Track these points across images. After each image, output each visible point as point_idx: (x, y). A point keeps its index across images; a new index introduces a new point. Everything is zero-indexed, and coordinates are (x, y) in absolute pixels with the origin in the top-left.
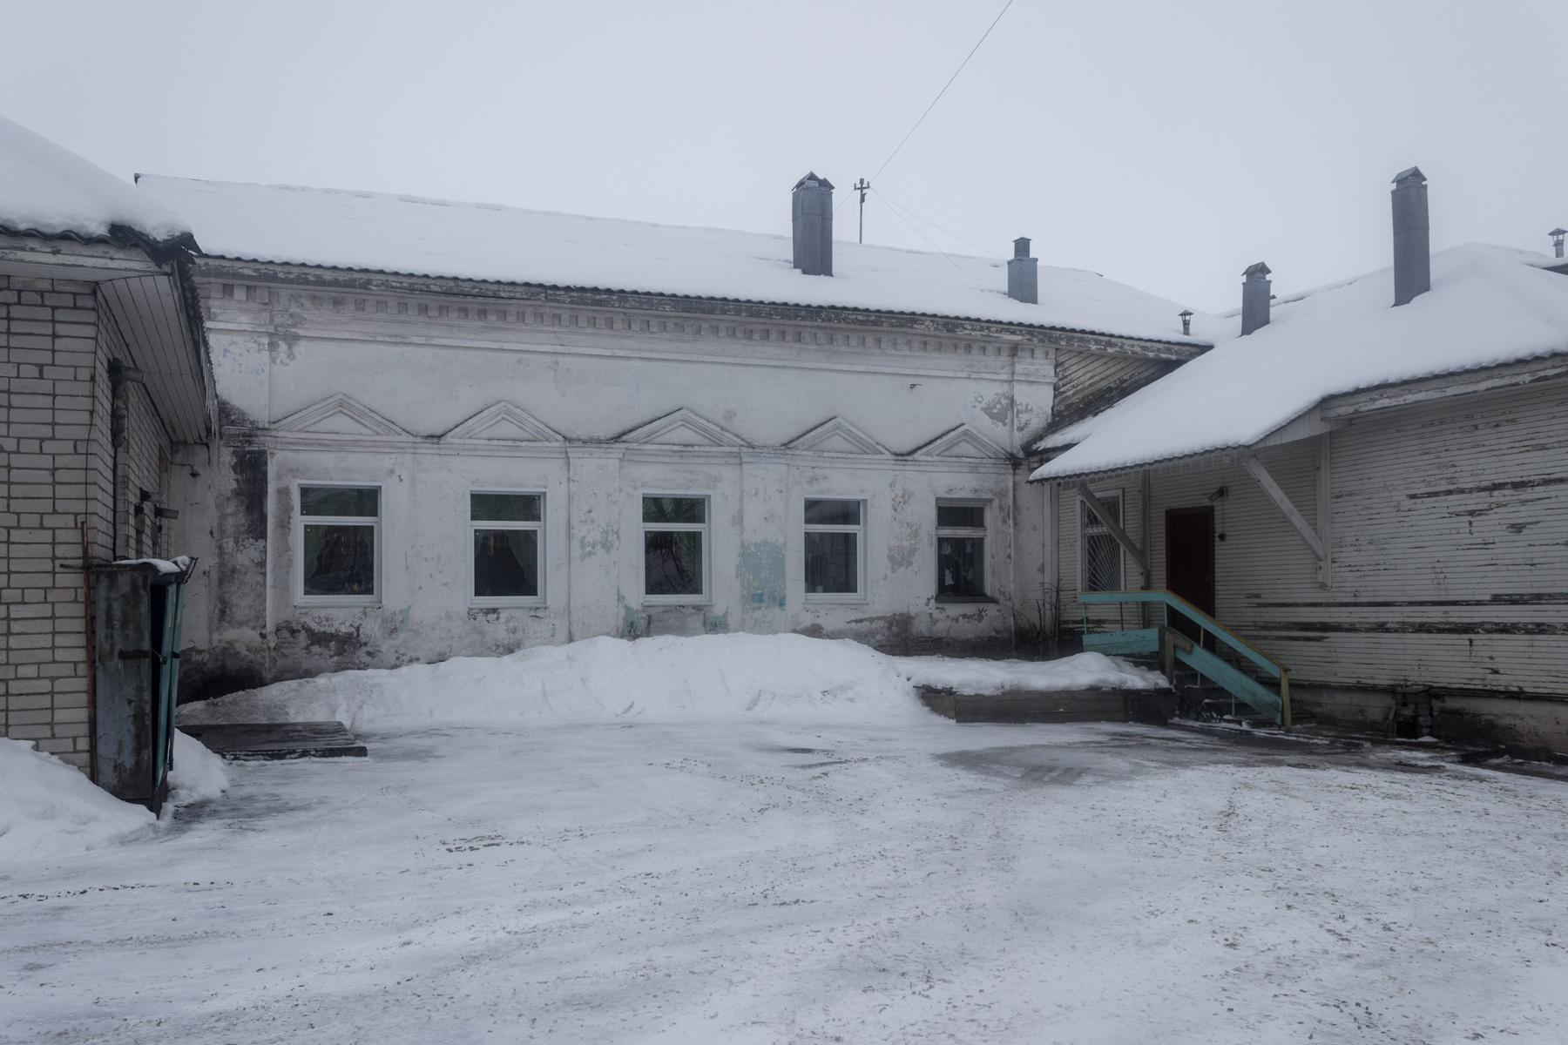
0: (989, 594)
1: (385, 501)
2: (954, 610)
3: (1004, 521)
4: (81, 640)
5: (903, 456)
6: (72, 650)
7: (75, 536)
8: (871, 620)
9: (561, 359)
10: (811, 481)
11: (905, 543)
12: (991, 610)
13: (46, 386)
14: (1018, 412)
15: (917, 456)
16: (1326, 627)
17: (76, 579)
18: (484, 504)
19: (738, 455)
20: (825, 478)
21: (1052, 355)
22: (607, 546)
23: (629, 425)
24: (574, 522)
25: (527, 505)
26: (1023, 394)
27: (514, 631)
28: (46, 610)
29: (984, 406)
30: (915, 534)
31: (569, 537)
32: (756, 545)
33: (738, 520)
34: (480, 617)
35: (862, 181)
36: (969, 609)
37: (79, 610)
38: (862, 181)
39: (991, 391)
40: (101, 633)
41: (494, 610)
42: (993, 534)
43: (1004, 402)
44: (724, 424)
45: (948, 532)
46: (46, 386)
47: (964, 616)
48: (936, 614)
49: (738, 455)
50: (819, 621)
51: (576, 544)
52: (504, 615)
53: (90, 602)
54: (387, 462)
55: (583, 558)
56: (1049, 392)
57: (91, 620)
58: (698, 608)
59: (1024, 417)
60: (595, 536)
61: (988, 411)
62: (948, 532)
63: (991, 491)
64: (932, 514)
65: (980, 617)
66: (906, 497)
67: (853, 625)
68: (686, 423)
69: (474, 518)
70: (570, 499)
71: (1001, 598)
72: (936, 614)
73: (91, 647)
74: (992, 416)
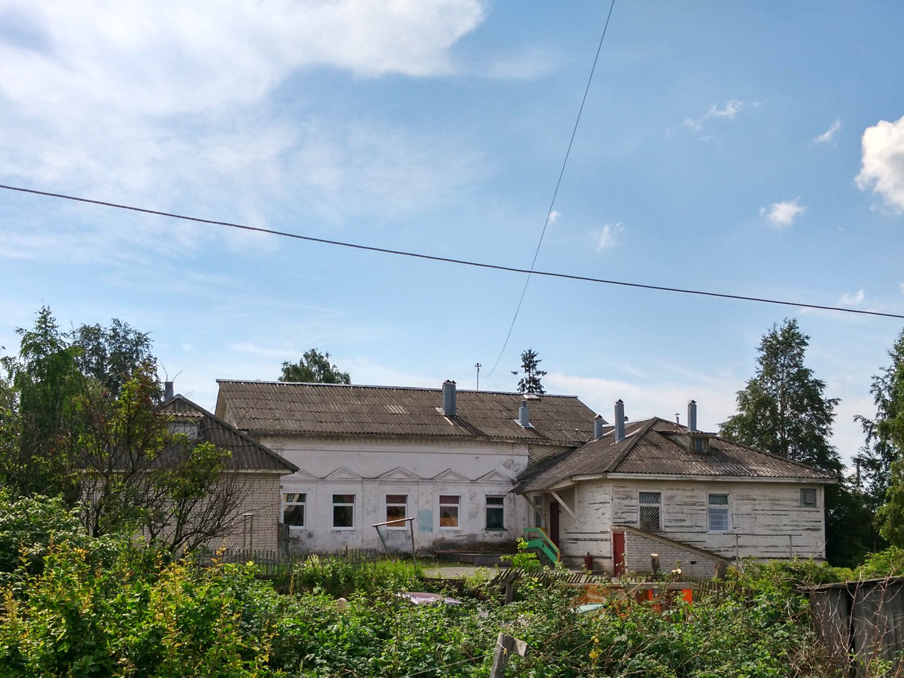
0: (505, 527)
1: (308, 498)
2: (492, 533)
3: (510, 503)
4: (277, 537)
5: (474, 481)
6: (275, 539)
7: (276, 518)
8: (462, 536)
9: (361, 453)
10: (442, 490)
11: (475, 510)
12: (505, 533)
13: (272, 492)
14: (515, 465)
15: (478, 481)
16: (577, 540)
17: (276, 526)
18: (337, 498)
19: (417, 482)
20: (446, 489)
21: (527, 446)
22: (374, 511)
23: (382, 473)
24: (364, 504)
25: (351, 498)
26: (517, 459)
27: (345, 538)
28: (271, 531)
29: (503, 463)
30: (478, 507)
31: (363, 508)
32: (423, 511)
33: (417, 502)
34: (335, 533)
35: (478, 364)
36: (497, 533)
37: (276, 531)
38: (478, 364)
39: (505, 459)
40: (280, 536)
41: (339, 531)
42: (506, 506)
43: (510, 462)
44: (413, 472)
45: (490, 506)
46: (272, 492)
47: (495, 535)
48: (485, 534)
49: (417, 482)
50: (444, 536)
51: (364, 511)
52: (342, 533)
53: (279, 530)
54: (308, 486)
55: (367, 515)
56: (526, 458)
57: (278, 533)
58: (403, 531)
59: (517, 467)
60: (371, 508)
61: (504, 465)
62: (490, 506)
63: (505, 492)
64: (484, 500)
65: (501, 535)
66: (475, 495)
67: (456, 538)
68: (401, 472)
69: (333, 502)
70: (363, 497)
71: (509, 529)
72: (485, 534)
73: (278, 538)
74: (506, 467)
